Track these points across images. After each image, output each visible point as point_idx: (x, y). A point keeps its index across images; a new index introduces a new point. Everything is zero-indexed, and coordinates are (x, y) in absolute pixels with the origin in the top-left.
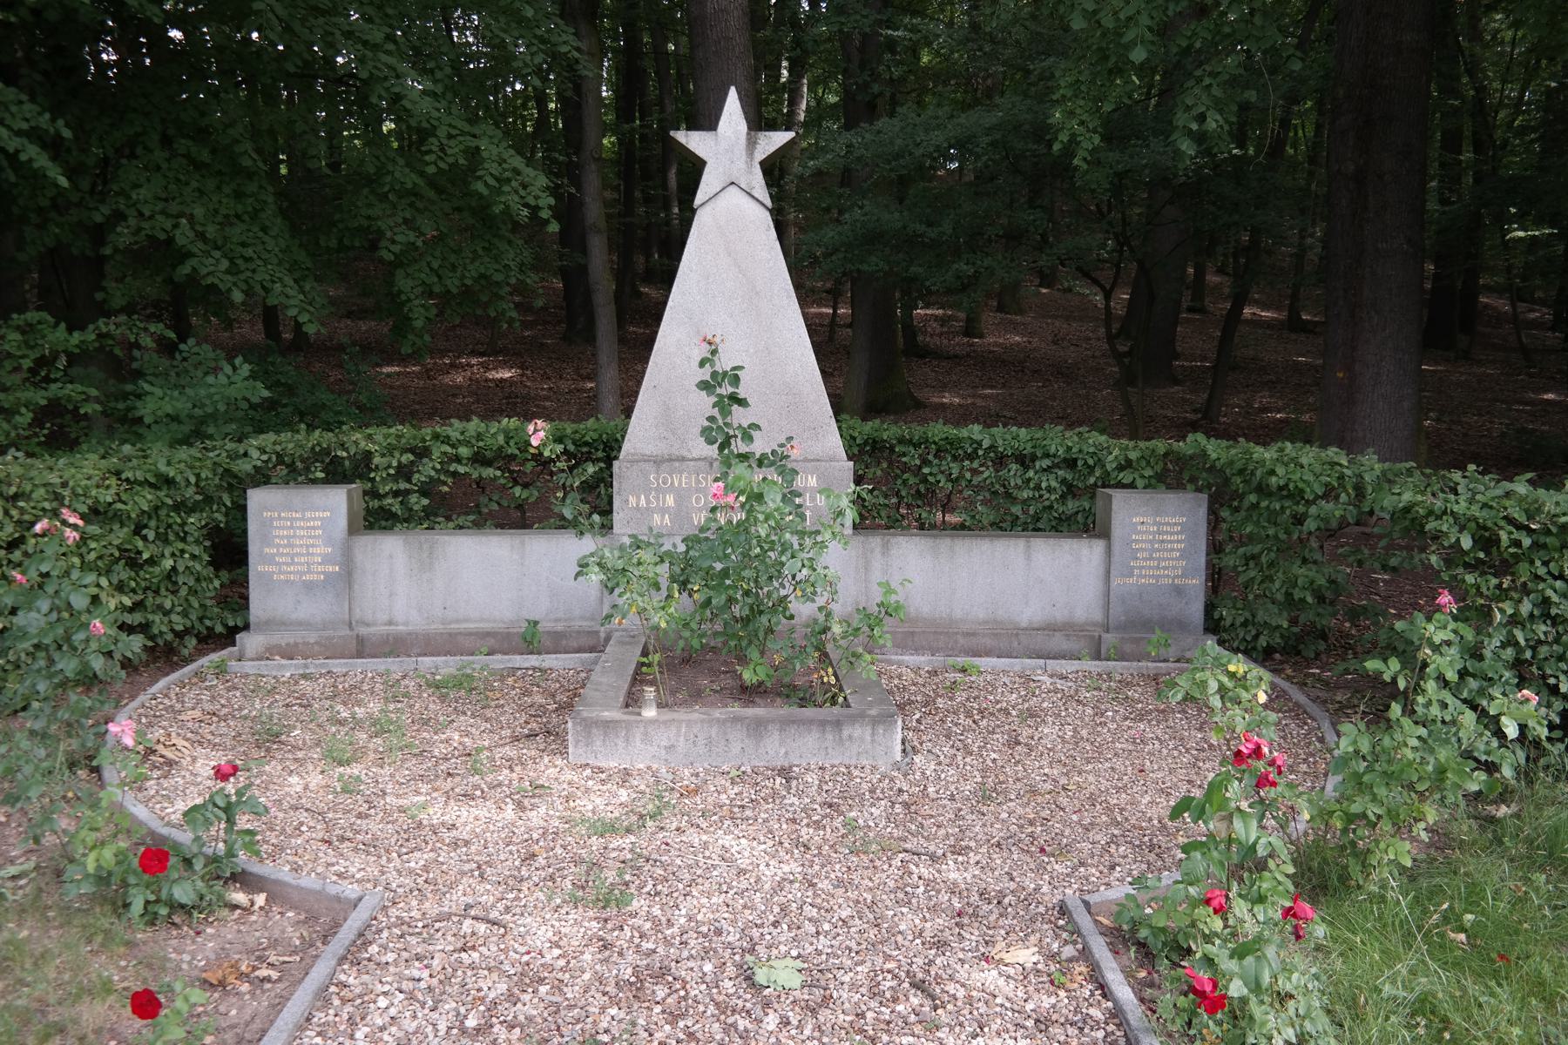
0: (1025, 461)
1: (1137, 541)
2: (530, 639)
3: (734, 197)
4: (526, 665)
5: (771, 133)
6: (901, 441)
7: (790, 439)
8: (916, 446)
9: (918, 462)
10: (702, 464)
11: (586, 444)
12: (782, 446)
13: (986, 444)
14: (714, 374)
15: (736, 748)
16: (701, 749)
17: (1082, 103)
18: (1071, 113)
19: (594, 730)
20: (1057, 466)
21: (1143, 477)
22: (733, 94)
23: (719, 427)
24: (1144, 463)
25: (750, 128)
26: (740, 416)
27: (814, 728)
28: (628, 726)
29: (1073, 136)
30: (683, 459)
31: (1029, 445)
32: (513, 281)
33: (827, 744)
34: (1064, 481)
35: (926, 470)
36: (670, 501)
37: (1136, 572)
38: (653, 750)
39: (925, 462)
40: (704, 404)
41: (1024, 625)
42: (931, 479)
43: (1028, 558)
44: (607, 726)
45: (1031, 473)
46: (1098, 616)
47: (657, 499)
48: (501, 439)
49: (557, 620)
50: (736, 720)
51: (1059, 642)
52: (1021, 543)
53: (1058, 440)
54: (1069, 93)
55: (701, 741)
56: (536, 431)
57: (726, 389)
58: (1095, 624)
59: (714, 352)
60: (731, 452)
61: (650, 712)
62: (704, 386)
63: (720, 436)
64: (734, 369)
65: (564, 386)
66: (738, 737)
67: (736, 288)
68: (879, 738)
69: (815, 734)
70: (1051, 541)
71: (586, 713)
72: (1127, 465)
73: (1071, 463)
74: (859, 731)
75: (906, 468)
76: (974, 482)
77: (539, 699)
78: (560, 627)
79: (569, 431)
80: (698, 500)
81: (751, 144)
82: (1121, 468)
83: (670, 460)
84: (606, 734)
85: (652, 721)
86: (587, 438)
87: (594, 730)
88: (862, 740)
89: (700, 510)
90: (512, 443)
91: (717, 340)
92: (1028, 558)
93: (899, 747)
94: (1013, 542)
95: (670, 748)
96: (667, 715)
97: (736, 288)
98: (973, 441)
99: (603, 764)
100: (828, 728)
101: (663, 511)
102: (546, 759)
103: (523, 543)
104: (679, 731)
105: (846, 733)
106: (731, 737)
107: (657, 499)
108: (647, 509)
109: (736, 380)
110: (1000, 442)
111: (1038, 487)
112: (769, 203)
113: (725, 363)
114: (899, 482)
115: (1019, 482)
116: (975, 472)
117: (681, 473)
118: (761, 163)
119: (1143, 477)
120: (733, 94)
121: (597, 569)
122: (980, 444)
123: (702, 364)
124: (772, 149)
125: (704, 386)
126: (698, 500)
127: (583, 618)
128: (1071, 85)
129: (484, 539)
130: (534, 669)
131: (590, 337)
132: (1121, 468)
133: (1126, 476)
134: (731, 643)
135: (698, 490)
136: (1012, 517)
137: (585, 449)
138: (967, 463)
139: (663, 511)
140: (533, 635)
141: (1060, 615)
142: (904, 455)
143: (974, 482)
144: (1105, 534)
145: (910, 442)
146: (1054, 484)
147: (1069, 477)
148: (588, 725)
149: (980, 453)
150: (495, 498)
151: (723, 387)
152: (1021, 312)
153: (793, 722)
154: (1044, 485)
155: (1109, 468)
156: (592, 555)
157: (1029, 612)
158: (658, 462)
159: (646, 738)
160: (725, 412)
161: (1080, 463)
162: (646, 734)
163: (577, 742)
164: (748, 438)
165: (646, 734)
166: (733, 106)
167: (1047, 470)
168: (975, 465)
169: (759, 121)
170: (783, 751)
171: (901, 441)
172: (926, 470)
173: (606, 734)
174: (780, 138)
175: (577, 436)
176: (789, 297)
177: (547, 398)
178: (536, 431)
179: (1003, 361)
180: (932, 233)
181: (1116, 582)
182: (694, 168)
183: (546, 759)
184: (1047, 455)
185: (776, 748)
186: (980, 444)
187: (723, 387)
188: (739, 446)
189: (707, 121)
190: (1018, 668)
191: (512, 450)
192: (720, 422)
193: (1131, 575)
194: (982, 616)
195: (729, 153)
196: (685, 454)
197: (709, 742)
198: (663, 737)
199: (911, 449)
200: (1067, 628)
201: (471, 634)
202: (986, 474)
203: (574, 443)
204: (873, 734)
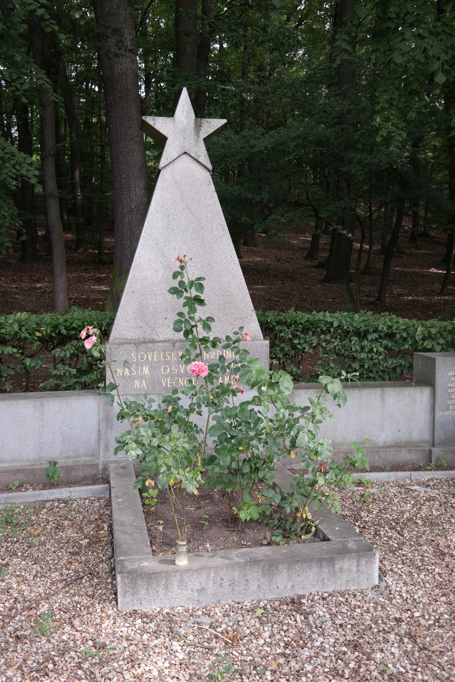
0: (362, 335)
1: (451, 388)
2: (51, 476)
3: (186, 161)
4: (52, 497)
5: (211, 120)
6: (278, 323)
7: (241, 328)
8: (289, 326)
9: (290, 336)
10: (167, 344)
11: (74, 329)
12: (236, 333)
13: (336, 324)
14: (181, 283)
15: (253, 586)
16: (226, 589)
17: (393, 112)
18: (388, 120)
19: (139, 582)
20: (381, 338)
21: (438, 344)
22: (185, 92)
23: (186, 320)
24: (438, 336)
25: (197, 116)
26: (201, 312)
27: (314, 565)
28: (168, 575)
29: (389, 133)
30: (153, 341)
31: (363, 325)
32: (7, 224)
33: (325, 576)
34: (386, 348)
35: (296, 341)
36: (146, 370)
37: (451, 407)
38: (187, 593)
39: (295, 336)
40: (178, 304)
41: (381, 444)
42: (299, 347)
43: (383, 400)
44: (150, 577)
45: (366, 342)
46: (427, 436)
47: (137, 369)
48: (16, 327)
49: (67, 458)
50: (253, 562)
51: (405, 456)
52: (378, 391)
53: (385, 321)
54: (387, 106)
55: (226, 583)
56: (88, 336)
57: (193, 293)
58: (424, 442)
59: (182, 268)
60: (194, 337)
61: (182, 561)
62: (174, 291)
63: (185, 327)
64: (199, 279)
65: (24, 285)
66: (255, 576)
67: (182, 226)
68: (362, 568)
69: (315, 569)
70: (397, 389)
71: (129, 566)
72: (429, 337)
73: (391, 336)
74: (347, 564)
75: (282, 340)
76: (328, 349)
77: (71, 533)
78: (70, 462)
79: (61, 320)
80: (165, 369)
81: (198, 127)
82: (424, 339)
83: (145, 342)
84: (149, 584)
85: (187, 570)
86: (74, 325)
87: (139, 582)
88: (350, 570)
89: (167, 376)
90: (23, 329)
91: (187, 259)
92: (383, 400)
93: (376, 573)
94: (373, 390)
95: (201, 591)
96: (199, 563)
97: (182, 226)
98: (327, 322)
99: (147, 609)
100: (324, 564)
101: (141, 378)
102: (98, 607)
103: (42, 405)
104: (208, 576)
105: (337, 566)
106: (249, 578)
107: (137, 369)
108: (130, 377)
109: (200, 288)
110: (344, 323)
111: (371, 351)
112: (210, 167)
113: (191, 274)
114: (278, 349)
115: (358, 348)
116: (328, 342)
117: (153, 351)
118: (205, 140)
119: (438, 344)
120: (185, 92)
121: (134, 445)
122: (331, 324)
123: (175, 275)
124: (212, 131)
125: (174, 291)
126: (165, 369)
127: (86, 455)
128: (387, 101)
129: (14, 403)
130: (58, 500)
131: (48, 258)
132: (424, 339)
133: (428, 344)
134: (238, 498)
135: (165, 363)
136: (372, 375)
137: (73, 332)
138: (322, 336)
139: (141, 378)
140: (54, 472)
141: (403, 437)
142: (281, 332)
143: (328, 349)
144: (428, 381)
145: (285, 323)
146: (381, 349)
147: (390, 344)
148: (136, 576)
149: (332, 330)
150: (12, 366)
151: (189, 292)
152: (256, 246)
153: (298, 561)
154: (375, 350)
155: (417, 338)
156: (129, 433)
157: (384, 436)
158: (137, 343)
159: (182, 584)
160: (193, 310)
161: (398, 336)
162: (182, 581)
163: (125, 593)
164: (207, 327)
165: (182, 581)
166: (185, 99)
167: (376, 340)
168: (328, 337)
169: (201, 110)
170: (290, 584)
171: (278, 323)
172: (296, 341)
173: (149, 584)
174: (217, 123)
175: (68, 324)
176: (223, 229)
177: (17, 293)
178: (88, 336)
179: (257, 271)
180: (258, 198)
181: (438, 414)
182: (160, 141)
183: (98, 607)
184: (375, 331)
185: (286, 584)
186: (331, 324)
187: (189, 292)
188: (200, 332)
189: (169, 110)
190: (392, 479)
191: (24, 334)
192: (187, 317)
193: (448, 409)
194: (354, 438)
195: (183, 131)
196: (155, 337)
197: (233, 583)
198: (195, 583)
199: (285, 328)
200: (408, 445)
201: (5, 472)
202: (336, 344)
203: (66, 328)
204: (358, 565)
